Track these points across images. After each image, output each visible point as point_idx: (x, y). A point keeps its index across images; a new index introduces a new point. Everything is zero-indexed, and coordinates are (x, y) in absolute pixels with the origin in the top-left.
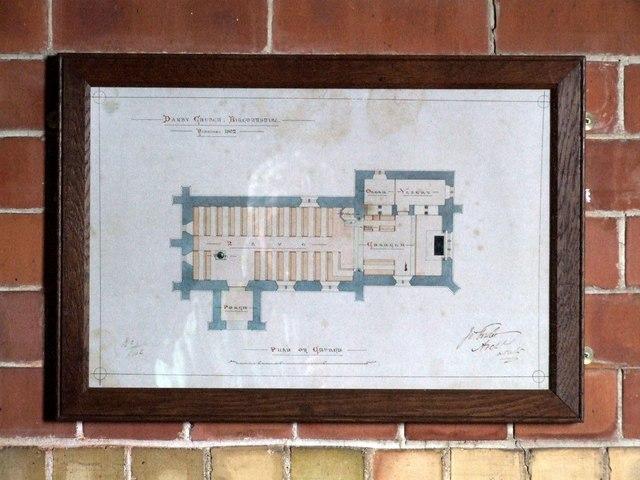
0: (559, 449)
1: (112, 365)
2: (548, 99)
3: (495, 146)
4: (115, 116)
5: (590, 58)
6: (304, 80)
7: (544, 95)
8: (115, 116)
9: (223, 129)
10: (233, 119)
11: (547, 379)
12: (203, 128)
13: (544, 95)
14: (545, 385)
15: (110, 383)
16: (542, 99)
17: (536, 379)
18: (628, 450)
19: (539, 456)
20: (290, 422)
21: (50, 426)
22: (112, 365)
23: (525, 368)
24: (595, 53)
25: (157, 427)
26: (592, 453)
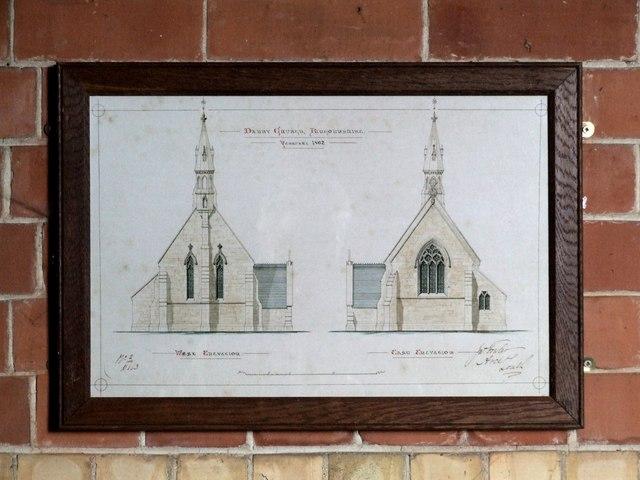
0: (60, 454)
1: (113, 373)
2: (545, 107)
3: (490, 161)
4: (116, 124)
5: (586, 65)
6: (101, 87)
7: (542, 101)
8: (116, 124)
9: (309, 141)
10: (314, 131)
11: (548, 386)
12: (287, 140)
13: (542, 101)
14: (545, 392)
15: (106, 394)
16: (539, 107)
17: (537, 385)
18: (157, 458)
19: (494, 457)
20: (245, 431)
21: (55, 436)
22: (113, 373)
23: (532, 380)
24: (599, 56)
25: (203, 436)
26: (555, 454)
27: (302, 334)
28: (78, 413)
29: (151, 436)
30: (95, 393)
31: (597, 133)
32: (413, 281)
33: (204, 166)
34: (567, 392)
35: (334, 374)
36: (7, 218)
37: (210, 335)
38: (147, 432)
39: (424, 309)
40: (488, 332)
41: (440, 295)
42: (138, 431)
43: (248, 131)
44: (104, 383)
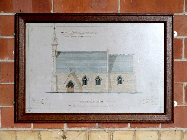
1: (31, 108)
3: (145, 43)
9: (79, 36)
12: (73, 36)
15: (31, 112)
21: (17, 124)
22: (31, 108)
27: (139, 94)
28: (22, 118)
29: (132, 125)
30: (27, 111)
31: (178, 35)
32: (82, 83)
33: (55, 43)
34: (169, 109)
35: (78, 106)
36: (183, 37)
37: (109, 94)
38: (34, 123)
39: (85, 88)
40: (141, 93)
41: (86, 86)
42: (31, 123)
43: (62, 33)
44: (160, 108)
